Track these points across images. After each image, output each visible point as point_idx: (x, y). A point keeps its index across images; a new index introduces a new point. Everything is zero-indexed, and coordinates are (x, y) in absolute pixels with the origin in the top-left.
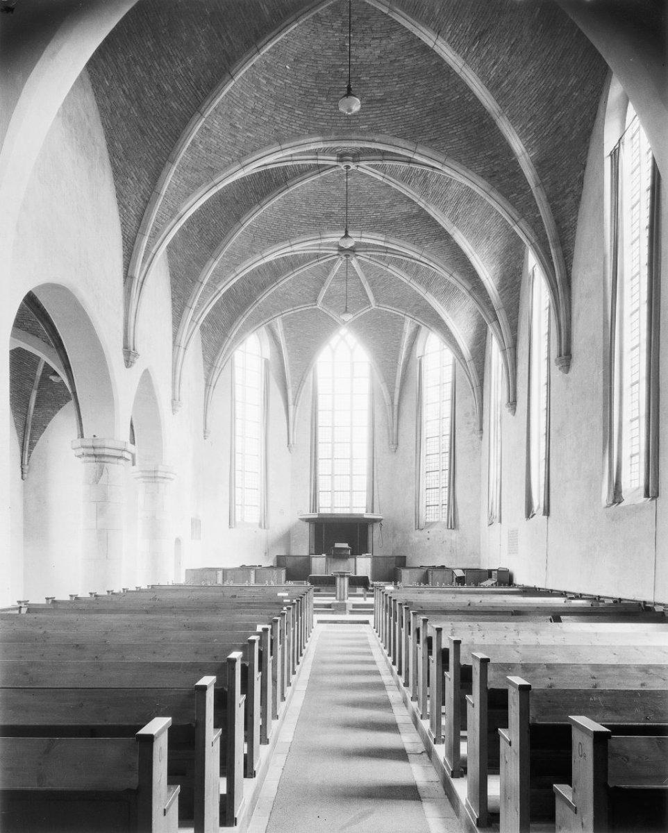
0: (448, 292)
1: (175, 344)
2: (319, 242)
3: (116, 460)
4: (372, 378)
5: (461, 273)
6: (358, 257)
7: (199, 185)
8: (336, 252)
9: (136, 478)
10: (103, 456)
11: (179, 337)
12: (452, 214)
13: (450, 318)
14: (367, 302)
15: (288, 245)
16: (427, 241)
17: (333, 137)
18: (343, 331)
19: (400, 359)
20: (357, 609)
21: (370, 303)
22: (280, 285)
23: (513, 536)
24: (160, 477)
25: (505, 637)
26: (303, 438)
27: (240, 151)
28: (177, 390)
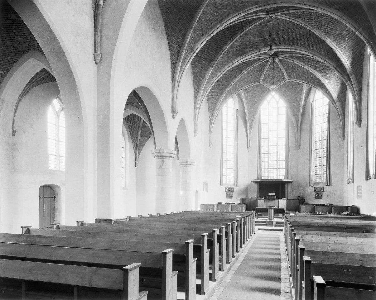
0: (324, 69)
1: (195, 106)
2: (259, 53)
3: (169, 158)
4: (287, 114)
5: (330, 59)
6: (279, 58)
7: (202, 36)
8: (268, 57)
9: (180, 165)
10: (163, 156)
11: (196, 104)
12: (325, 31)
13: (326, 82)
14: (285, 78)
15: (244, 56)
16: (313, 46)
17: (262, 4)
18: (273, 93)
19: (301, 104)
20: (278, 224)
21: (285, 79)
22: (242, 75)
23: (360, 189)
24: (189, 165)
25: (330, 239)
26: (254, 144)
27: (220, 18)
28: (196, 126)
